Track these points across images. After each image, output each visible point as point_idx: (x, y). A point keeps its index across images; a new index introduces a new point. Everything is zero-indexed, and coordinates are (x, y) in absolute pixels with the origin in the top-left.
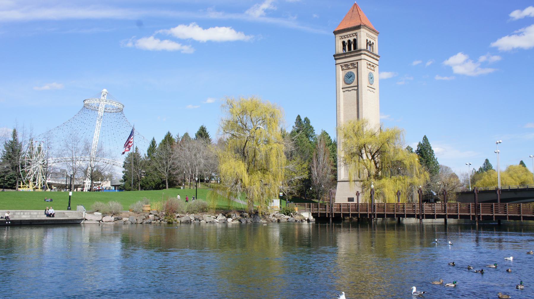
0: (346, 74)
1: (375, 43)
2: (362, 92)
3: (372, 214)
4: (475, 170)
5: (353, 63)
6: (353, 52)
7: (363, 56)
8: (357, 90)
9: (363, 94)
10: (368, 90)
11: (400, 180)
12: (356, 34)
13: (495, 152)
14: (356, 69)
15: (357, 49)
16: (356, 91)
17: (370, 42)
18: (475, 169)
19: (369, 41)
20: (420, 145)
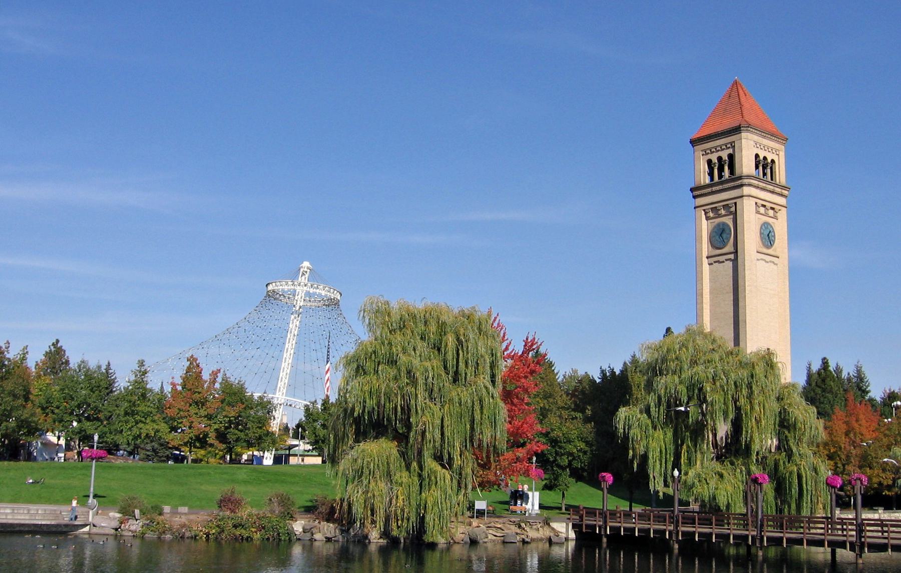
6: (727, 181)
7: (746, 190)
8: (735, 261)
10: (758, 260)
17: (765, 158)
19: (761, 158)
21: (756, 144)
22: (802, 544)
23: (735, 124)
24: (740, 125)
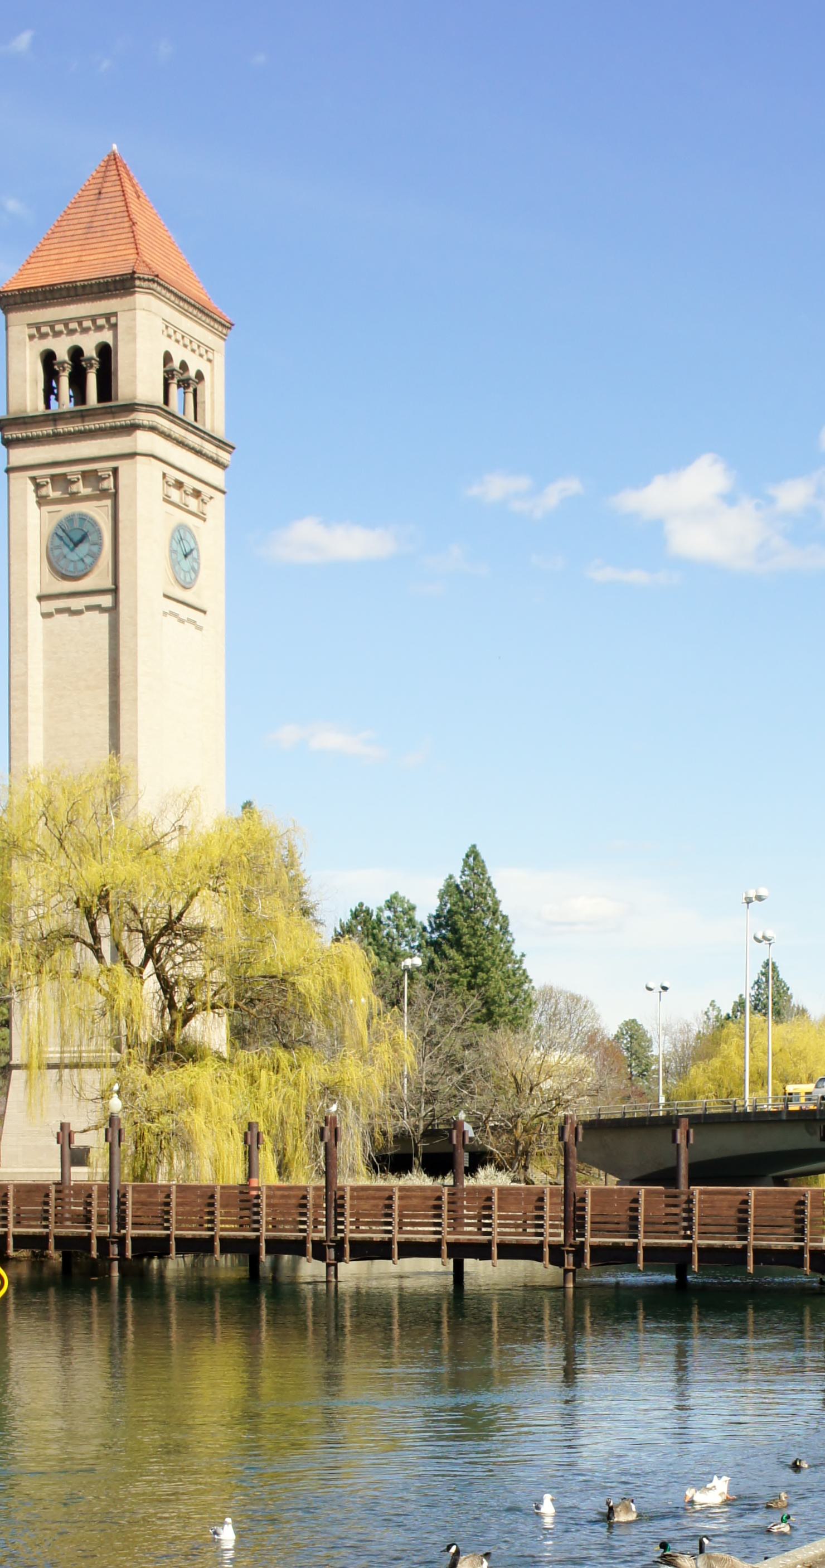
0: (60, 526)
1: (213, 375)
2: (136, 625)
3: (112, 1236)
4: (719, 1011)
5: (96, 471)
6: (92, 413)
7: (143, 440)
8: (114, 610)
9: (140, 632)
10: (165, 614)
11: (277, 1070)
12: (113, 320)
13: (755, 938)
14: (108, 502)
15: (117, 399)
16: (105, 617)
17: (184, 366)
18: (717, 1004)
19: (176, 364)
20: (451, 890)
21: (167, 327)
22: (211, 1251)
23: (119, 268)
24: (134, 272)
